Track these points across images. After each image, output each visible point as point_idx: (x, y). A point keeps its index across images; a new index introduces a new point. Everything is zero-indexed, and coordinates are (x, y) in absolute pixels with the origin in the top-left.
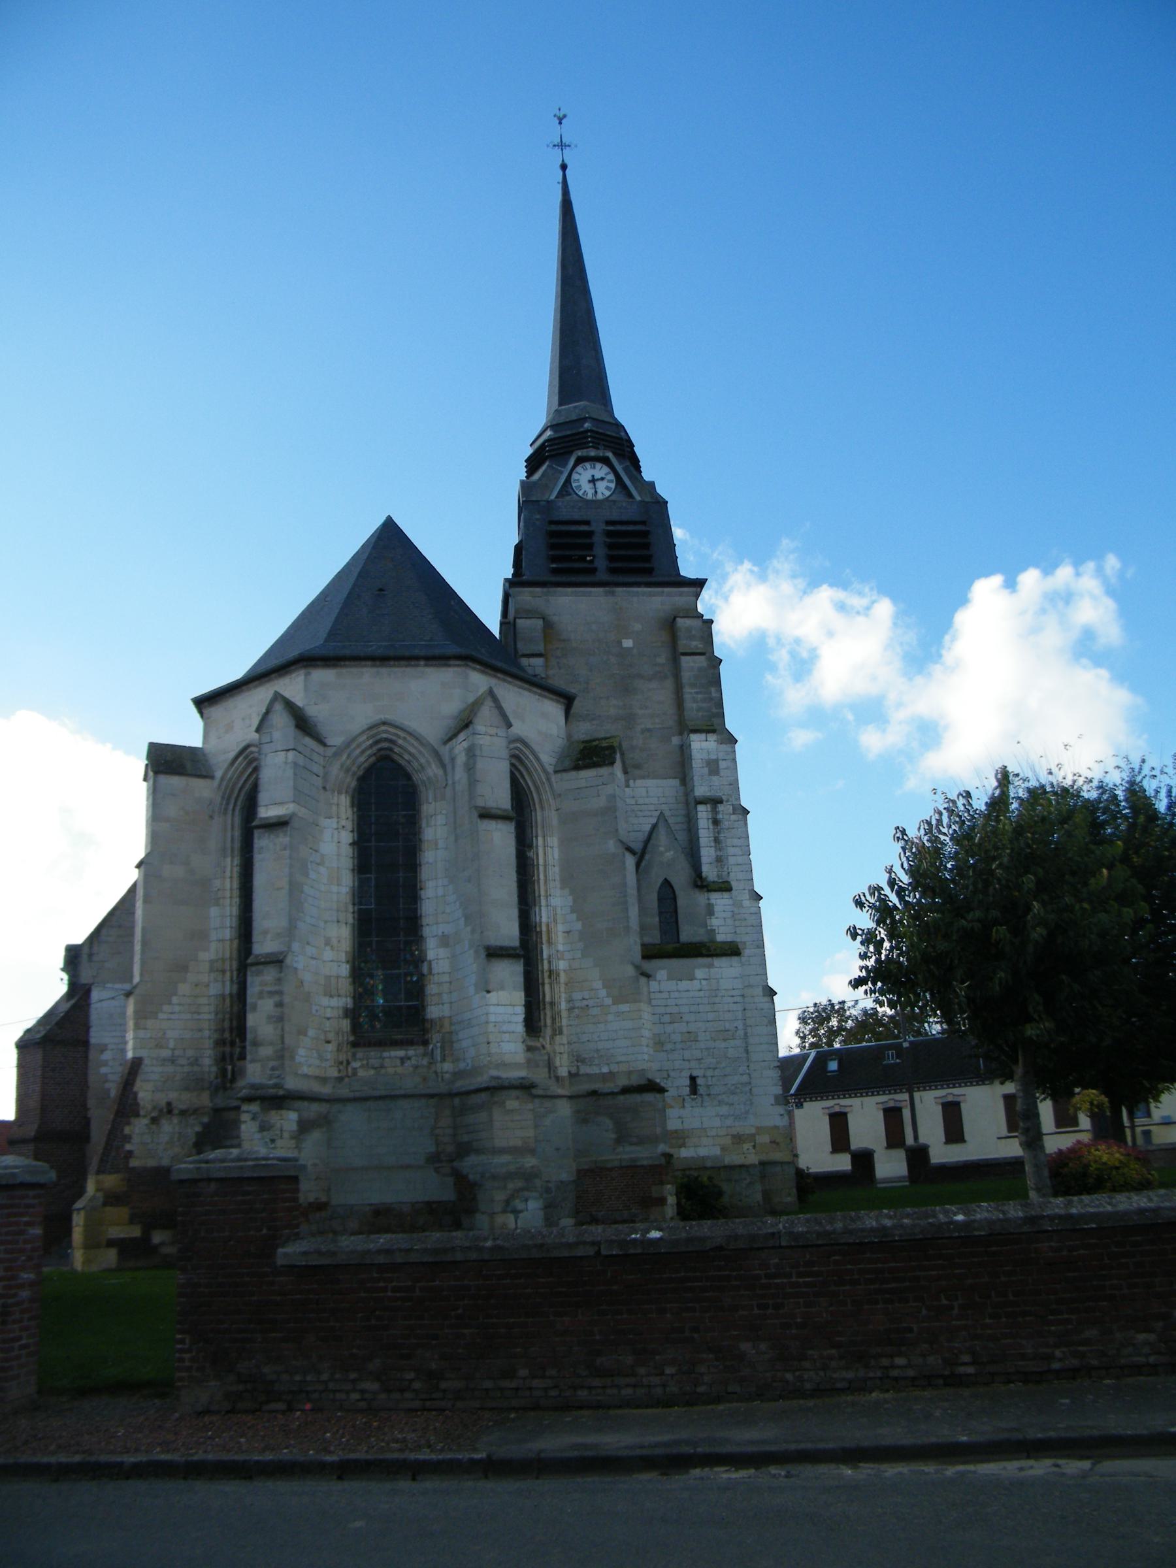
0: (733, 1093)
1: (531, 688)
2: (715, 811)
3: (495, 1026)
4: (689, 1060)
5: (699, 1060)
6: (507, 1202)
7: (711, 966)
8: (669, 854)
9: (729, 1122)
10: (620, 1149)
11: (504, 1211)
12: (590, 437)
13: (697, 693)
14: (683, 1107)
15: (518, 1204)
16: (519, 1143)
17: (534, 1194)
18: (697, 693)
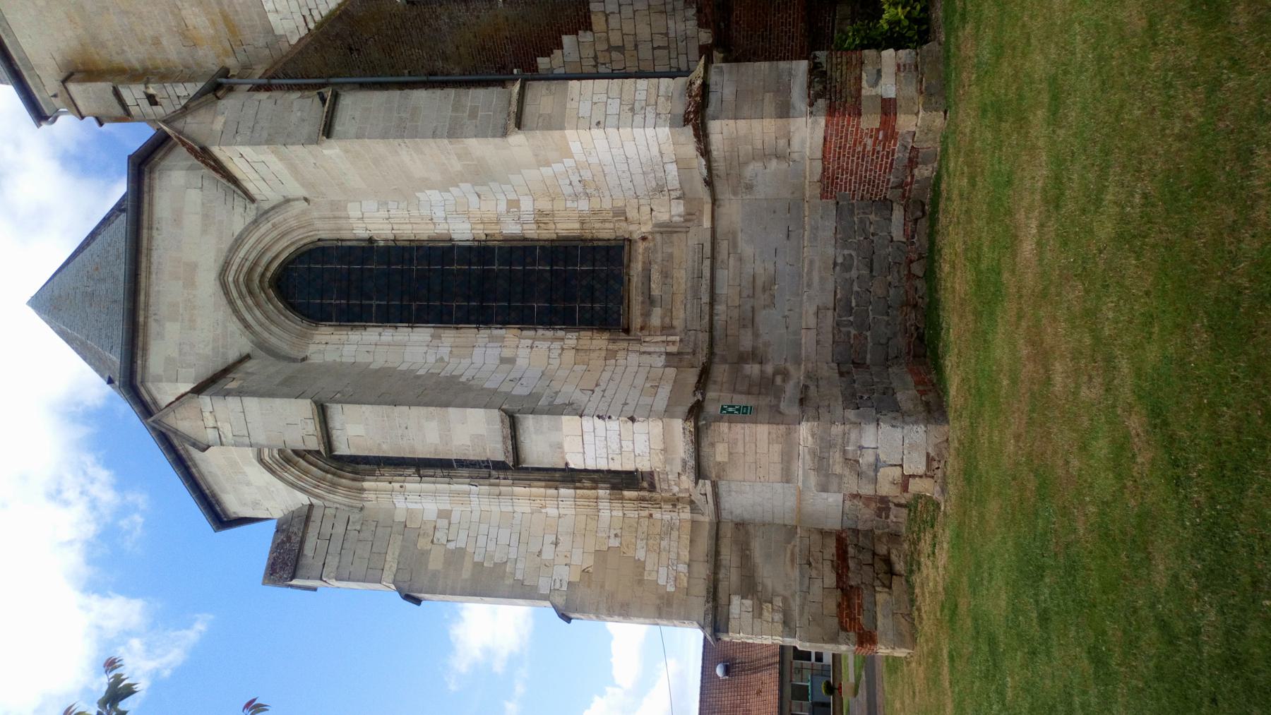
1: (144, 251)
3: (613, 459)
11: (875, 481)
15: (867, 459)
16: (777, 448)
17: (853, 435)
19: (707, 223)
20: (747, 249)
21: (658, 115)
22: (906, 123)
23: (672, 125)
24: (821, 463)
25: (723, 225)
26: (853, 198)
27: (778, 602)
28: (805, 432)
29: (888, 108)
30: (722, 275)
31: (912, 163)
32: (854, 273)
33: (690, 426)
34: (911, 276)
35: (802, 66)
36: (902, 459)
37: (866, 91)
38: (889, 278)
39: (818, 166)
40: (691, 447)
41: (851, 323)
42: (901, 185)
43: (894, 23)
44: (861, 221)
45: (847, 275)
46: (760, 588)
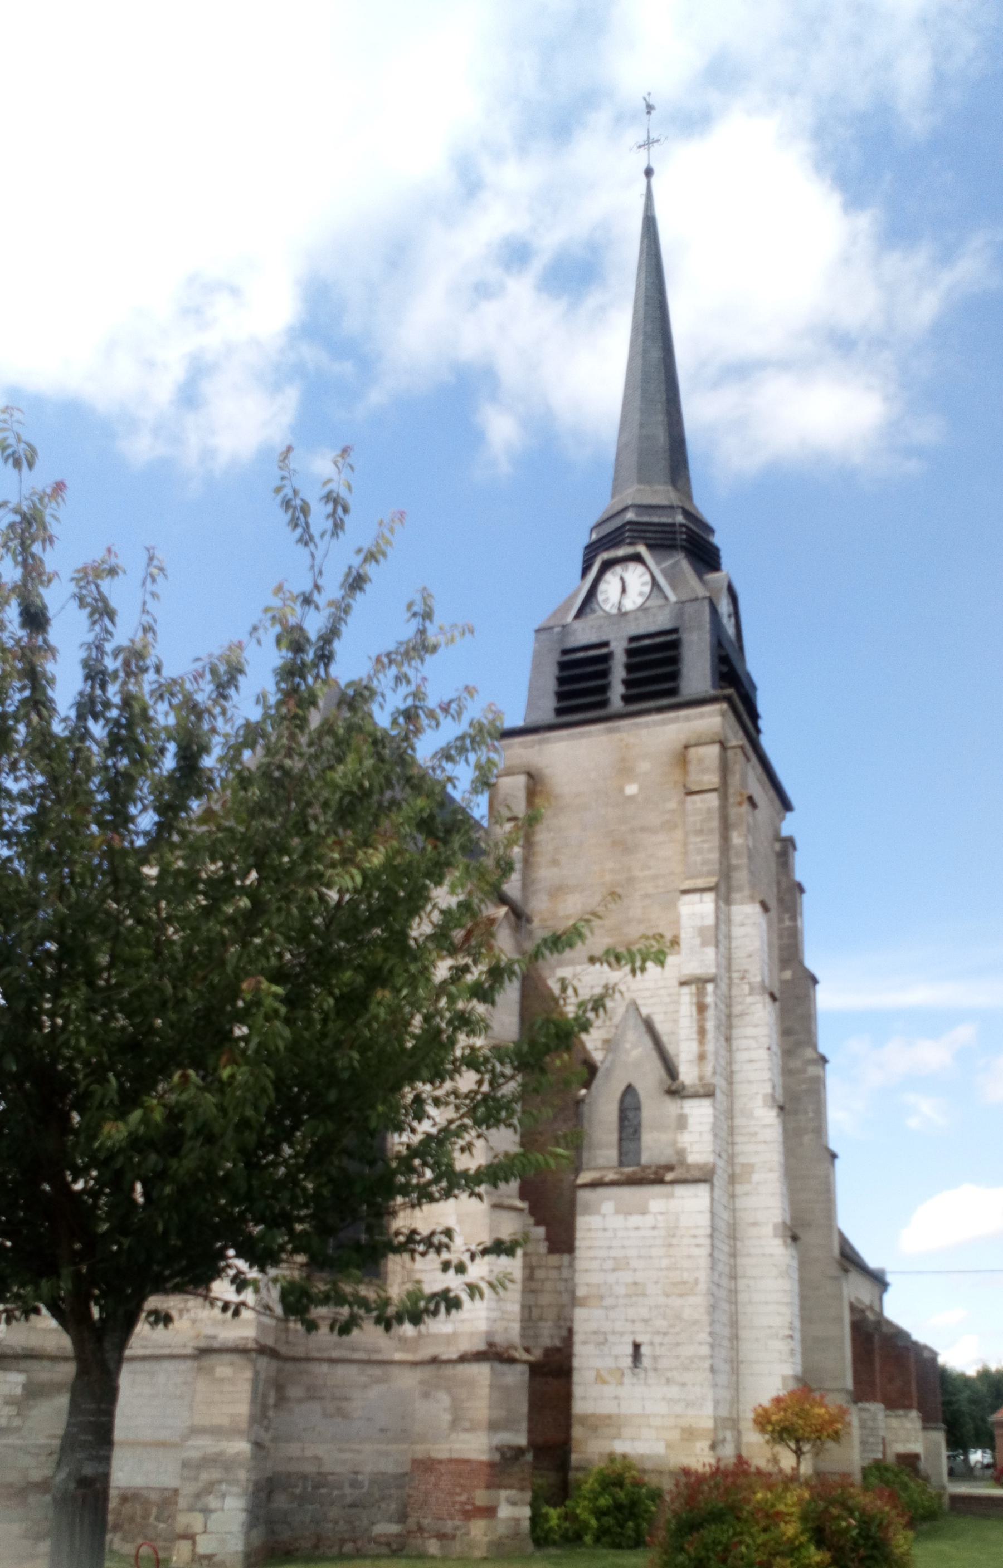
0: (687, 1369)
2: (701, 993)
4: (633, 1321)
5: (645, 1321)
6: (198, 1496)
7: (671, 1196)
8: (636, 1053)
9: (679, 1409)
10: (454, 1436)
11: (191, 1509)
12: (629, 530)
13: (703, 842)
14: (621, 1384)
15: (212, 1502)
16: (225, 1422)
17: (235, 1489)
18: (703, 842)
19: (398, 1356)
20: (374, 1392)
21: (495, 1321)
22: (478, 1528)
23: (489, 1334)
24: (208, 1461)
25: (395, 1370)
26: (410, 1488)
27: (17, 1422)
28: (241, 1447)
29: (489, 1512)
30: (353, 1370)
31: (441, 1536)
32: (348, 1490)
33: (251, 1345)
34: (343, 1542)
35: (521, 1440)
36: (212, 1533)
37: (504, 1494)
38: (342, 1522)
39: (444, 1455)
40: (230, 1344)
41: (305, 1489)
42: (421, 1529)
43: (546, 1517)
44: (391, 1496)
45: (347, 1485)
46: (31, 1403)
